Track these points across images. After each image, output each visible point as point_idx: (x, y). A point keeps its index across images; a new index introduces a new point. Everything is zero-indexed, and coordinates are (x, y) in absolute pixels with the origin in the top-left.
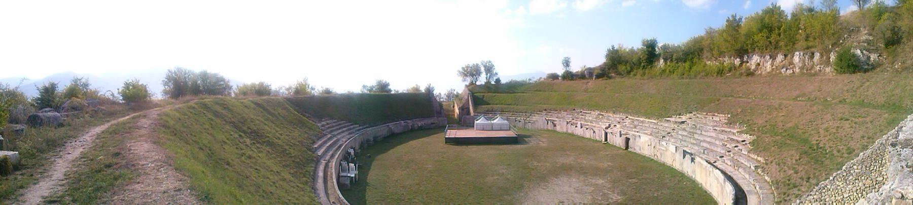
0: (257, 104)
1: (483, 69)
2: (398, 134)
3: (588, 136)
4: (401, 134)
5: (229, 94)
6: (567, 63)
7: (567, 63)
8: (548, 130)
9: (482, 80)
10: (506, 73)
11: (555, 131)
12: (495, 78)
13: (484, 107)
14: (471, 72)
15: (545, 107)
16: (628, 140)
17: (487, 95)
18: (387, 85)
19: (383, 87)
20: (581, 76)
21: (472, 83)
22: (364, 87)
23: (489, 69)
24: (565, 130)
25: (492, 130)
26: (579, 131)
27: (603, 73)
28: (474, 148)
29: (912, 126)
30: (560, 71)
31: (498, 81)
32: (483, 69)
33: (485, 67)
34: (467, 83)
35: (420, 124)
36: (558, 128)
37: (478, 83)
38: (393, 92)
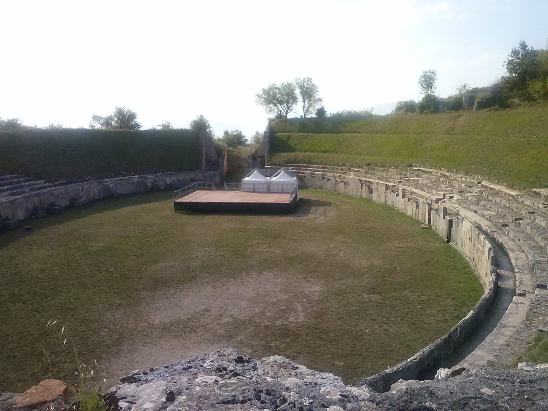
0: (135, 403)
1: (297, 92)
2: (121, 196)
3: (409, 213)
4: (128, 195)
5: (132, 122)
6: (428, 81)
7: (428, 81)
8: (361, 198)
9: (297, 111)
10: (336, 102)
11: (369, 201)
12: (318, 106)
13: (285, 156)
14: (277, 97)
15: (369, 159)
16: (451, 223)
17: (302, 140)
18: (132, 116)
19: (126, 120)
20: (457, 105)
21: (280, 117)
22: (95, 118)
23: (308, 93)
24: (383, 200)
25: (254, 192)
26: (400, 203)
27: (496, 99)
28: (209, 219)
29: (1, 127)
30: (417, 96)
31: (321, 112)
32: (297, 92)
33: (302, 87)
34: (273, 116)
35: (169, 181)
36: (375, 196)
37: (290, 116)
38: (143, 129)
